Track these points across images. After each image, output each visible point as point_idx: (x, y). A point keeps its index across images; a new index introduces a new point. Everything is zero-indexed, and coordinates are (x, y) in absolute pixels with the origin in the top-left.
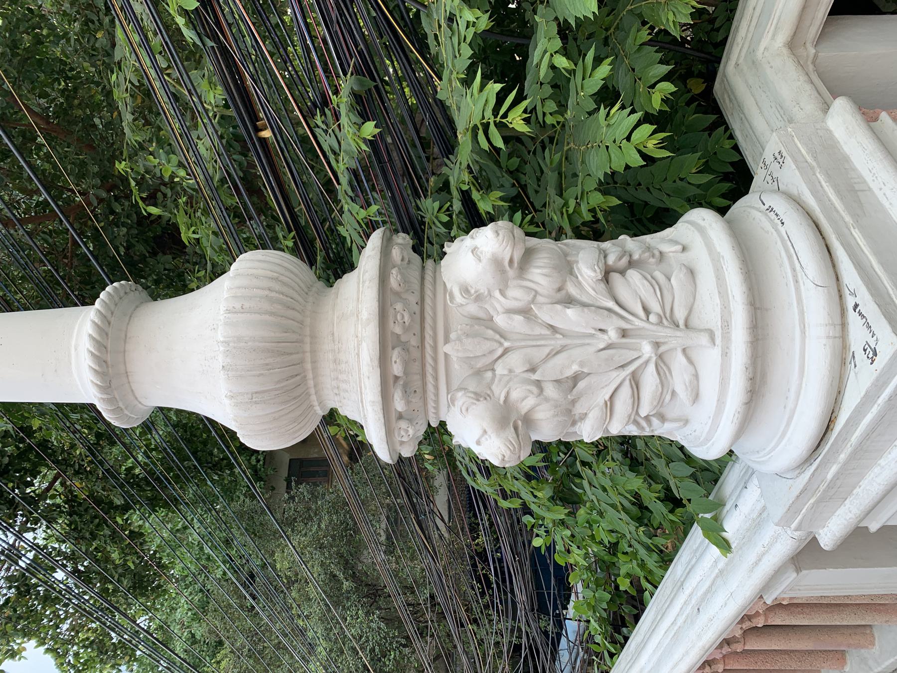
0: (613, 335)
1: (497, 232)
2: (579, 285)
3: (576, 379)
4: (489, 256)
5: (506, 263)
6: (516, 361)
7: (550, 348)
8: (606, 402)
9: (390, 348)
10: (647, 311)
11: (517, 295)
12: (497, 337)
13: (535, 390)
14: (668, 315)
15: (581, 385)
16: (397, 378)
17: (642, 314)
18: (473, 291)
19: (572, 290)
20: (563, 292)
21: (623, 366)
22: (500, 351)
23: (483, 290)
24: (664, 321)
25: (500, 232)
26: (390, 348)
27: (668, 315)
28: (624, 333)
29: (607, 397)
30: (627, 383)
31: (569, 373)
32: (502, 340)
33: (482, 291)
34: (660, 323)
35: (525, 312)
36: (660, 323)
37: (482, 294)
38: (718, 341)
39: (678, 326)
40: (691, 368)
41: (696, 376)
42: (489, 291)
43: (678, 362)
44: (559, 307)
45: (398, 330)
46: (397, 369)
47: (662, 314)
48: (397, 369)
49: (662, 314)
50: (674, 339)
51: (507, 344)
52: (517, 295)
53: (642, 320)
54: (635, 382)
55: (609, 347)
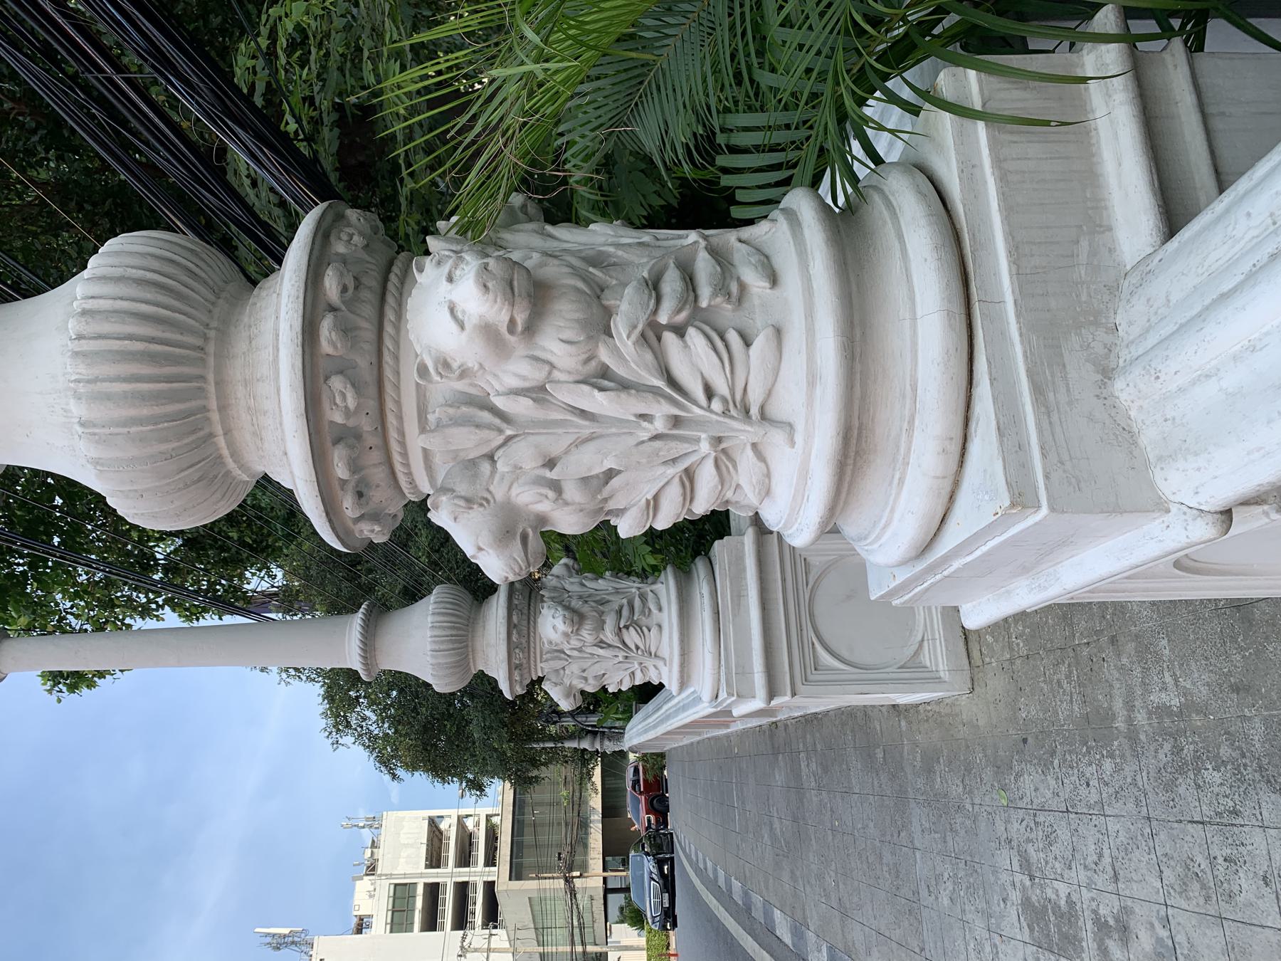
0: (659, 426)
1: (485, 286)
2: (616, 352)
3: (610, 474)
4: (475, 320)
5: (504, 330)
6: (524, 454)
7: (575, 436)
8: (648, 502)
9: (329, 444)
10: (710, 393)
11: (517, 371)
12: (497, 421)
13: (551, 494)
14: (738, 397)
15: (615, 482)
16: (343, 483)
17: (700, 395)
18: (455, 365)
19: (604, 356)
20: (593, 363)
21: (674, 460)
22: (501, 439)
23: (472, 363)
24: (733, 412)
25: (490, 285)
26: (329, 444)
27: (738, 397)
28: (676, 421)
29: (650, 497)
30: (677, 480)
31: (598, 470)
32: (504, 426)
33: (470, 365)
34: (726, 413)
35: (538, 393)
36: (726, 413)
37: (468, 369)
38: (799, 438)
39: (747, 412)
40: (762, 465)
41: (768, 475)
42: (481, 365)
43: (746, 460)
44: (586, 388)
45: (338, 418)
46: (341, 470)
47: (729, 398)
48: (341, 470)
49: (729, 398)
50: (742, 434)
51: (509, 432)
52: (517, 371)
53: (701, 407)
54: (689, 476)
55: (656, 437)
